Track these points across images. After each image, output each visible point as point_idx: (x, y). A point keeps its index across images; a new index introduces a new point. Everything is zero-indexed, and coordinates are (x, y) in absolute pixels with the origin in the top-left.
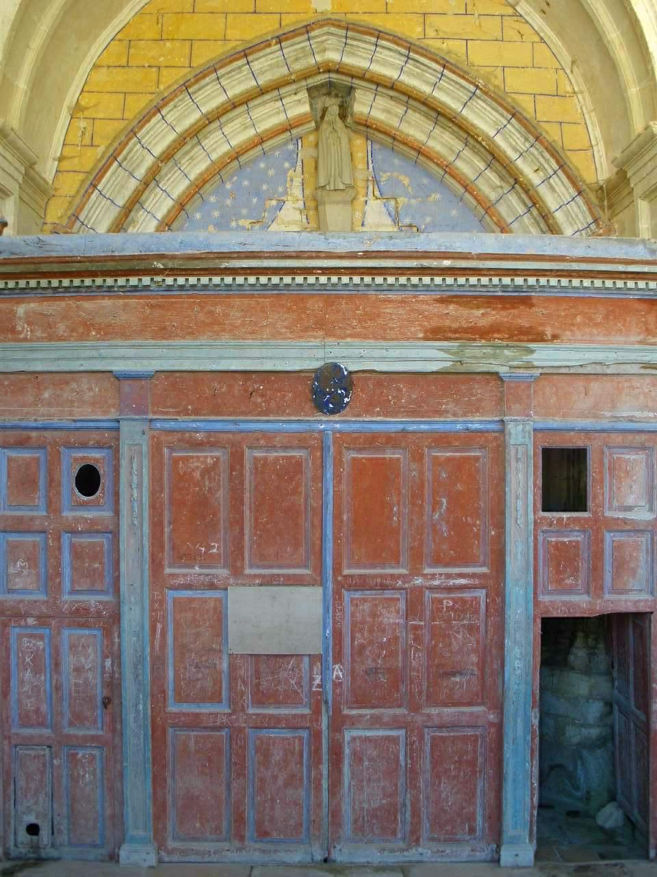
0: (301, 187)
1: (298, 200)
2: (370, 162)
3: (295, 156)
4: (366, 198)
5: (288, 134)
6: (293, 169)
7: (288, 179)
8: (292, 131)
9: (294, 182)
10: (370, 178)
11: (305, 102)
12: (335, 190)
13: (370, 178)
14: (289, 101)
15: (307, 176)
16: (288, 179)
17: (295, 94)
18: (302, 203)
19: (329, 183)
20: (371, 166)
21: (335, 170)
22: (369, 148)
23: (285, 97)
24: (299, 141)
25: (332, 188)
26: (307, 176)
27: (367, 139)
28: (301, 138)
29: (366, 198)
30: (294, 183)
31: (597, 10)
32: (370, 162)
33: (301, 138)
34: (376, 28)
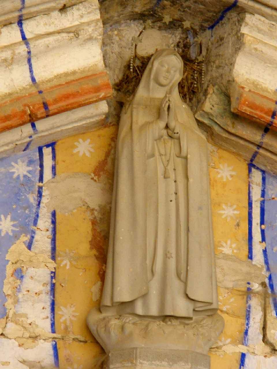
0: (47, 299)
1: (35, 338)
2: (257, 236)
3: (32, 198)
4: (242, 349)
5: (27, 129)
6: (25, 238)
7: (9, 269)
8: (39, 125)
9: (26, 280)
10: (256, 287)
11: (90, 39)
12: (165, 318)
13: (256, 287)
14: (42, 30)
15: (66, 263)
16: (9, 269)
17: (63, 9)
18: (48, 346)
19: (145, 296)
20: (258, 248)
21: (166, 256)
22: (256, 196)
23: (32, 16)
24: (47, 152)
25: (154, 311)
26: (66, 263)
27: (251, 166)
28: (52, 145)
29: (242, 349)
30: (28, 283)
31: (176, 59)
32: (257, 236)
33: (52, 145)
34: (31, 19)
